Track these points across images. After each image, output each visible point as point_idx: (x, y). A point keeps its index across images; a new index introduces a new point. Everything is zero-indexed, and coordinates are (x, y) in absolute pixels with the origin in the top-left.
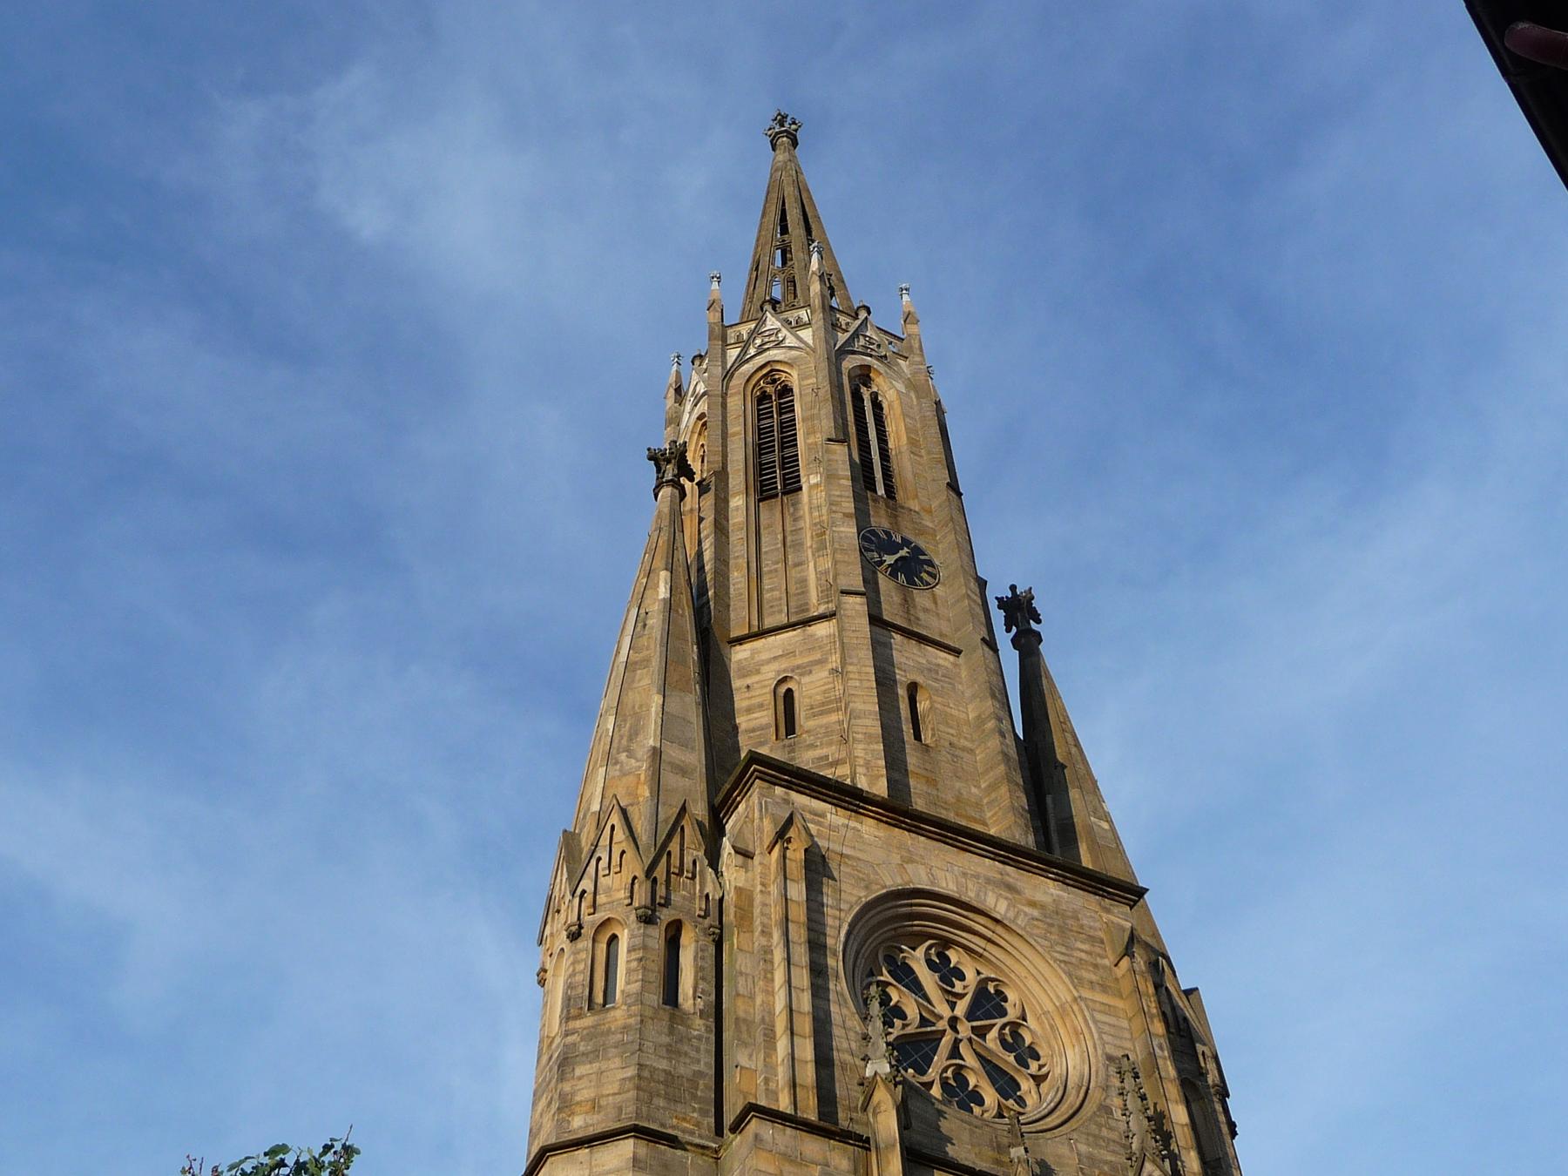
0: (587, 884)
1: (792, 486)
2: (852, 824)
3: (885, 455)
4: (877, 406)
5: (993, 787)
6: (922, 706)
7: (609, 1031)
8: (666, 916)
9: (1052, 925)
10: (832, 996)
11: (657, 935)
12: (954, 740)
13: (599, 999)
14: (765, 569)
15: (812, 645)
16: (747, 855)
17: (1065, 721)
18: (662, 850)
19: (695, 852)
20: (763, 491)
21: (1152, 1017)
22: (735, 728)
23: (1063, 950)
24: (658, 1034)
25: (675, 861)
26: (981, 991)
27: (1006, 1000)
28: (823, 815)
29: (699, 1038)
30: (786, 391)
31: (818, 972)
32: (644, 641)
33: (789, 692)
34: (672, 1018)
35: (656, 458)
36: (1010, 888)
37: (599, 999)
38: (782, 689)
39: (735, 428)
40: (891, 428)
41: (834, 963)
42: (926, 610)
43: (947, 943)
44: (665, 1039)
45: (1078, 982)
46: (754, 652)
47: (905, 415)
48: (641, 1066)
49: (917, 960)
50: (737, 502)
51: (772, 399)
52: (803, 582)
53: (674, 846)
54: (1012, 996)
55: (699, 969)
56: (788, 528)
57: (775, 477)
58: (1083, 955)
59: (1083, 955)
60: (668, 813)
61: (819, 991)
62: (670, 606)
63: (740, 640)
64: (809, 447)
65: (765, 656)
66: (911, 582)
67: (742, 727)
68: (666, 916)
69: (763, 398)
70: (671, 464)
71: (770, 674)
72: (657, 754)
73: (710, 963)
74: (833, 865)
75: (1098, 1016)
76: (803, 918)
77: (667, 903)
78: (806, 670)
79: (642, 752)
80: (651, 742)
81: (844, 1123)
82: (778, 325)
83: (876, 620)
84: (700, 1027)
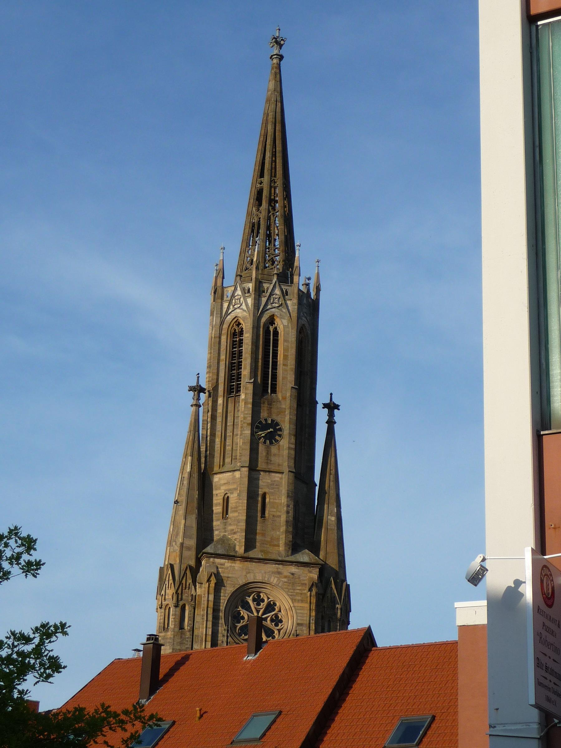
0: (163, 592)
2: (233, 565)
3: (275, 364)
4: (276, 333)
7: (167, 638)
8: (181, 603)
9: (290, 583)
10: (220, 625)
11: (178, 609)
12: (274, 514)
13: (166, 627)
14: (228, 434)
16: (202, 584)
18: (181, 583)
19: (190, 581)
21: (313, 610)
22: (213, 511)
23: (292, 591)
24: (178, 640)
25: (184, 586)
26: (269, 604)
27: (276, 605)
28: (223, 564)
29: (188, 638)
31: (216, 618)
32: (182, 491)
33: (228, 497)
34: (182, 633)
35: (192, 389)
36: (279, 573)
37: (166, 627)
38: (226, 496)
39: (223, 357)
41: (222, 614)
42: (275, 455)
43: (260, 592)
44: (179, 640)
45: (293, 600)
46: (220, 479)
48: (173, 649)
49: (250, 600)
50: (220, 401)
53: (184, 581)
54: (278, 604)
55: (189, 617)
56: (236, 415)
57: (233, 389)
58: (298, 591)
59: (298, 591)
60: (184, 567)
61: (215, 624)
62: (190, 474)
63: (216, 474)
65: (222, 482)
66: (271, 443)
67: (214, 512)
68: (181, 603)
69: (234, 334)
70: (198, 390)
72: (182, 544)
73: (192, 615)
74: (225, 582)
75: (298, 611)
76: (212, 606)
77: (181, 599)
78: (232, 491)
79: (178, 544)
80: (277, 204)
84: (188, 634)
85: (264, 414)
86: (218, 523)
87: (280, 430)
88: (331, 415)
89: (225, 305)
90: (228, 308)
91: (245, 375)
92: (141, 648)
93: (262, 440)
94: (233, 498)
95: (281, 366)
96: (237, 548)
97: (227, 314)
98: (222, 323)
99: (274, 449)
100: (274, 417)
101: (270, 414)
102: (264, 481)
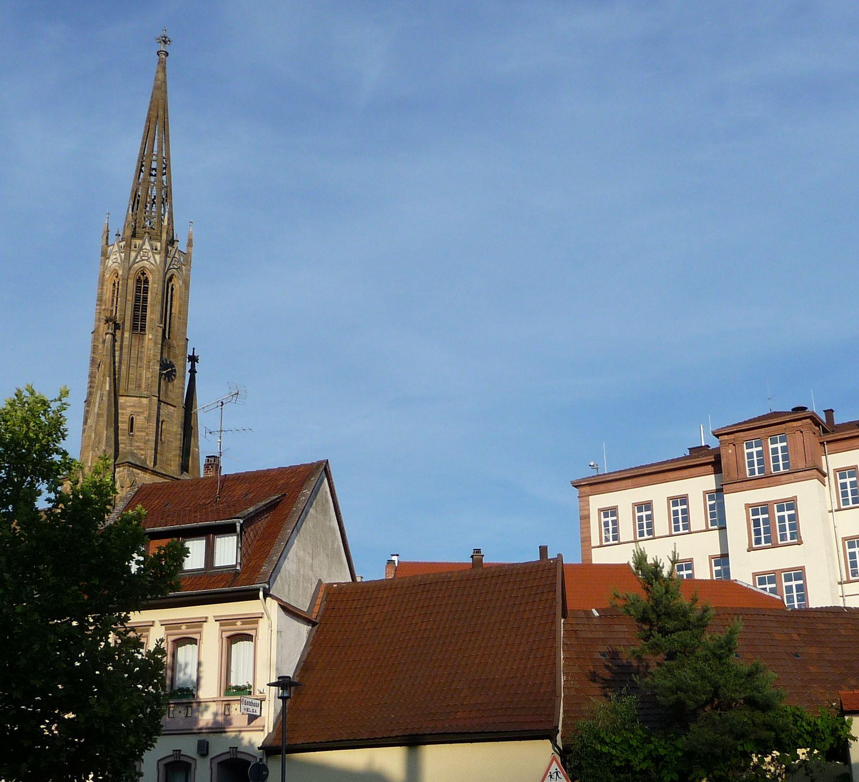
1: (143, 328)
5: (175, 456)
6: (164, 427)
15: (141, 405)
17: (196, 414)
20: (134, 327)
30: (146, 281)
39: (129, 298)
40: (174, 303)
47: (180, 298)
51: (142, 283)
52: (141, 374)
57: (139, 325)
62: (109, 392)
64: (152, 320)
65: (128, 404)
71: (129, 411)
78: (139, 414)
81: (117, 470)
82: (149, 248)
83: (159, 400)
85: (165, 356)
86: (124, 438)
87: (175, 371)
88: (193, 366)
89: (133, 254)
90: (136, 257)
91: (152, 320)
92: (551, 555)
93: (163, 376)
94: (139, 421)
95: (177, 319)
96: (148, 463)
97: (134, 262)
98: (130, 268)
99: (170, 385)
100: (172, 360)
101: (169, 355)
102: (165, 409)
